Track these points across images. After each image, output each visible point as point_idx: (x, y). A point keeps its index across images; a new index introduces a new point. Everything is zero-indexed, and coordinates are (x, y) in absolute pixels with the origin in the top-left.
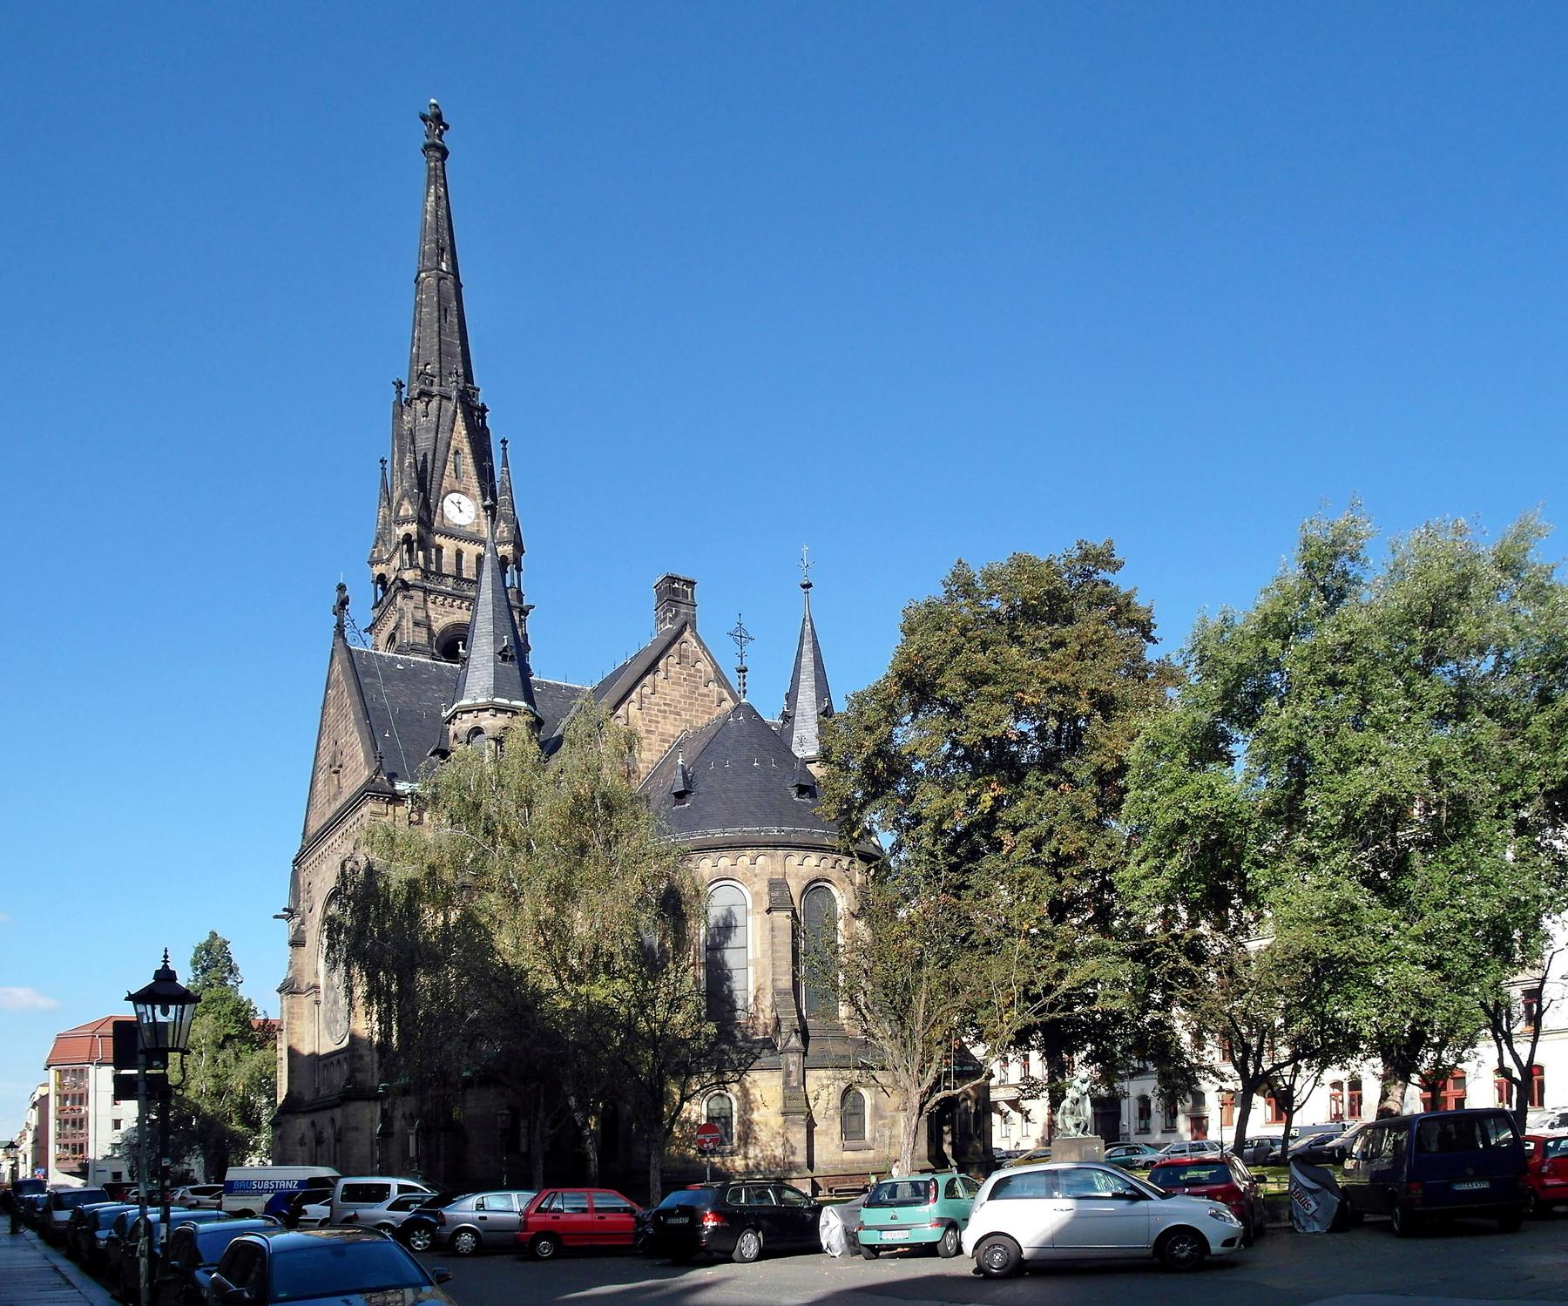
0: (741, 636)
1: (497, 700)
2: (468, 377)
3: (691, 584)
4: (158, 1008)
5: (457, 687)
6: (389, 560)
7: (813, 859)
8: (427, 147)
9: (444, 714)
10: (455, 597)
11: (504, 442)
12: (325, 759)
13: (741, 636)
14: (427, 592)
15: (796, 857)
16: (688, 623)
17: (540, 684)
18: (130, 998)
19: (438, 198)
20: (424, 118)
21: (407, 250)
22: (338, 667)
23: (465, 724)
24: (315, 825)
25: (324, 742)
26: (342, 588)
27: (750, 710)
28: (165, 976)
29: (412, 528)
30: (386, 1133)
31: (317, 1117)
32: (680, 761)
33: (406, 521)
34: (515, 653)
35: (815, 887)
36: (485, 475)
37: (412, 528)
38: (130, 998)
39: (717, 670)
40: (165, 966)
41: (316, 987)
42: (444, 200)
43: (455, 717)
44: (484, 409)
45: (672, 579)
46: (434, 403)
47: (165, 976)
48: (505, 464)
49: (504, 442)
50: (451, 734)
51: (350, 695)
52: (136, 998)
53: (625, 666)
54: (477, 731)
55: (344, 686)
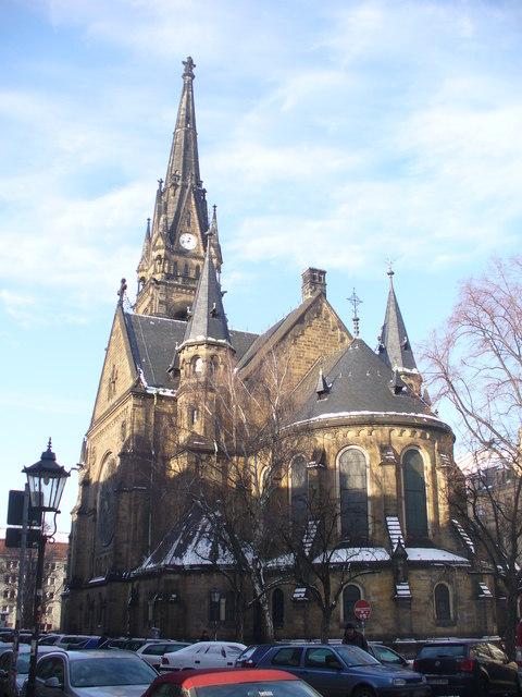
0: (355, 300)
1: (210, 339)
2: (197, 175)
3: (324, 273)
4: (42, 480)
5: (181, 334)
6: (147, 271)
7: (408, 432)
8: (184, 75)
9: (177, 348)
10: (183, 287)
11: (215, 207)
12: (108, 375)
13: (355, 300)
14: (166, 284)
15: (396, 432)
16: (323, 294)
17: (232, 332)
18: (26, 470)
19: (188, 96)
20: (184, 63)
21: (170, 116)
22: (118, 323)
23: (186, 355)
24: (99, 413)
25: (107, 365)
26: (124, 281)
27: (362, 343)
28: (48, 456)
29: (162, 252)
30: (135, 603)
31: (90, 591)
32: (321, 373)
33: (159, 248)
34: (217, 315)
35: (411, 452)
36: (204, 225)
37: (162, 252)
38: (26, 470)
39: (340, 321)
40: (49, 450)
41: (95, 510)
42: (190, 100)
43: (183, 348)
44: (204, 191)
45: (312, 270)
46: (179, 190)
47: (48, 456)
48: (215, 217)
49: (215, 207)
50: (181, 359)
51: (125, 338)
52: (30, 471)
53: (283, 321)
54: (196, 358)
55: (121, 333)
